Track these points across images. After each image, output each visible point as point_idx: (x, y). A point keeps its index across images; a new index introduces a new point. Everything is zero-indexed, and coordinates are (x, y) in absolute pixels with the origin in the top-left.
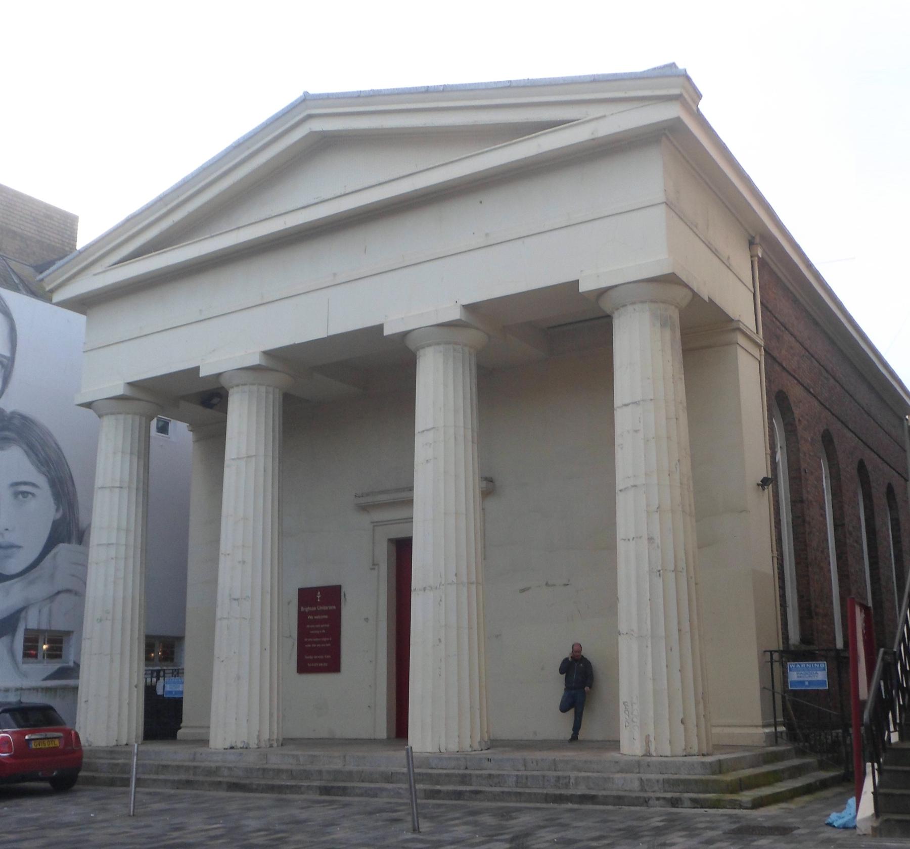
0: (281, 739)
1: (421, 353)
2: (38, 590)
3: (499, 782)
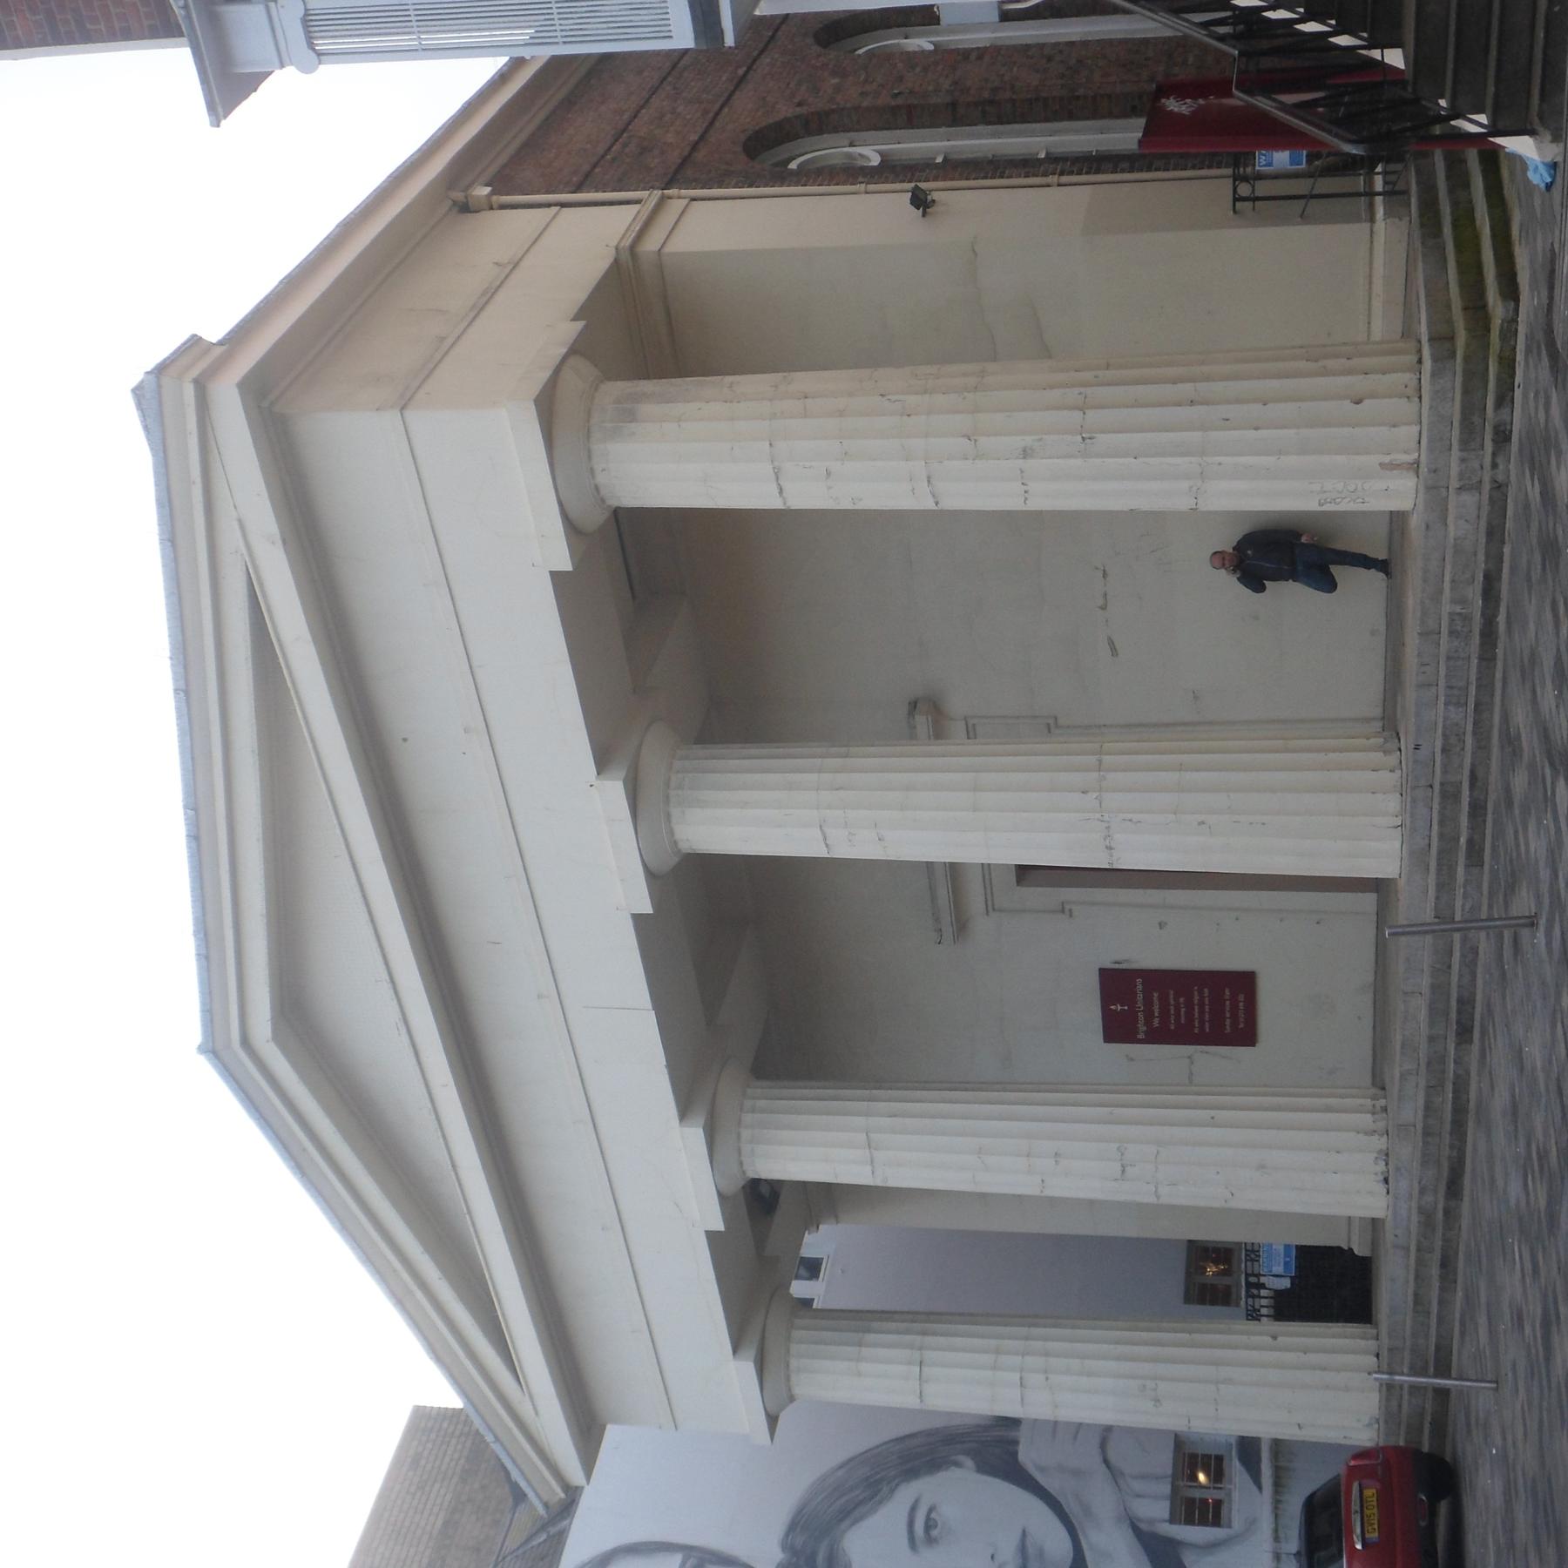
0: (1374, 1091)
1: (685, 847)
2: (1101, 1499)
3: (1457, 735)
